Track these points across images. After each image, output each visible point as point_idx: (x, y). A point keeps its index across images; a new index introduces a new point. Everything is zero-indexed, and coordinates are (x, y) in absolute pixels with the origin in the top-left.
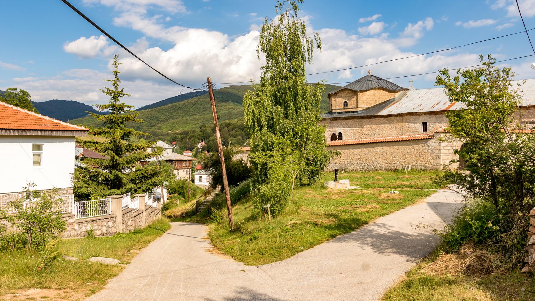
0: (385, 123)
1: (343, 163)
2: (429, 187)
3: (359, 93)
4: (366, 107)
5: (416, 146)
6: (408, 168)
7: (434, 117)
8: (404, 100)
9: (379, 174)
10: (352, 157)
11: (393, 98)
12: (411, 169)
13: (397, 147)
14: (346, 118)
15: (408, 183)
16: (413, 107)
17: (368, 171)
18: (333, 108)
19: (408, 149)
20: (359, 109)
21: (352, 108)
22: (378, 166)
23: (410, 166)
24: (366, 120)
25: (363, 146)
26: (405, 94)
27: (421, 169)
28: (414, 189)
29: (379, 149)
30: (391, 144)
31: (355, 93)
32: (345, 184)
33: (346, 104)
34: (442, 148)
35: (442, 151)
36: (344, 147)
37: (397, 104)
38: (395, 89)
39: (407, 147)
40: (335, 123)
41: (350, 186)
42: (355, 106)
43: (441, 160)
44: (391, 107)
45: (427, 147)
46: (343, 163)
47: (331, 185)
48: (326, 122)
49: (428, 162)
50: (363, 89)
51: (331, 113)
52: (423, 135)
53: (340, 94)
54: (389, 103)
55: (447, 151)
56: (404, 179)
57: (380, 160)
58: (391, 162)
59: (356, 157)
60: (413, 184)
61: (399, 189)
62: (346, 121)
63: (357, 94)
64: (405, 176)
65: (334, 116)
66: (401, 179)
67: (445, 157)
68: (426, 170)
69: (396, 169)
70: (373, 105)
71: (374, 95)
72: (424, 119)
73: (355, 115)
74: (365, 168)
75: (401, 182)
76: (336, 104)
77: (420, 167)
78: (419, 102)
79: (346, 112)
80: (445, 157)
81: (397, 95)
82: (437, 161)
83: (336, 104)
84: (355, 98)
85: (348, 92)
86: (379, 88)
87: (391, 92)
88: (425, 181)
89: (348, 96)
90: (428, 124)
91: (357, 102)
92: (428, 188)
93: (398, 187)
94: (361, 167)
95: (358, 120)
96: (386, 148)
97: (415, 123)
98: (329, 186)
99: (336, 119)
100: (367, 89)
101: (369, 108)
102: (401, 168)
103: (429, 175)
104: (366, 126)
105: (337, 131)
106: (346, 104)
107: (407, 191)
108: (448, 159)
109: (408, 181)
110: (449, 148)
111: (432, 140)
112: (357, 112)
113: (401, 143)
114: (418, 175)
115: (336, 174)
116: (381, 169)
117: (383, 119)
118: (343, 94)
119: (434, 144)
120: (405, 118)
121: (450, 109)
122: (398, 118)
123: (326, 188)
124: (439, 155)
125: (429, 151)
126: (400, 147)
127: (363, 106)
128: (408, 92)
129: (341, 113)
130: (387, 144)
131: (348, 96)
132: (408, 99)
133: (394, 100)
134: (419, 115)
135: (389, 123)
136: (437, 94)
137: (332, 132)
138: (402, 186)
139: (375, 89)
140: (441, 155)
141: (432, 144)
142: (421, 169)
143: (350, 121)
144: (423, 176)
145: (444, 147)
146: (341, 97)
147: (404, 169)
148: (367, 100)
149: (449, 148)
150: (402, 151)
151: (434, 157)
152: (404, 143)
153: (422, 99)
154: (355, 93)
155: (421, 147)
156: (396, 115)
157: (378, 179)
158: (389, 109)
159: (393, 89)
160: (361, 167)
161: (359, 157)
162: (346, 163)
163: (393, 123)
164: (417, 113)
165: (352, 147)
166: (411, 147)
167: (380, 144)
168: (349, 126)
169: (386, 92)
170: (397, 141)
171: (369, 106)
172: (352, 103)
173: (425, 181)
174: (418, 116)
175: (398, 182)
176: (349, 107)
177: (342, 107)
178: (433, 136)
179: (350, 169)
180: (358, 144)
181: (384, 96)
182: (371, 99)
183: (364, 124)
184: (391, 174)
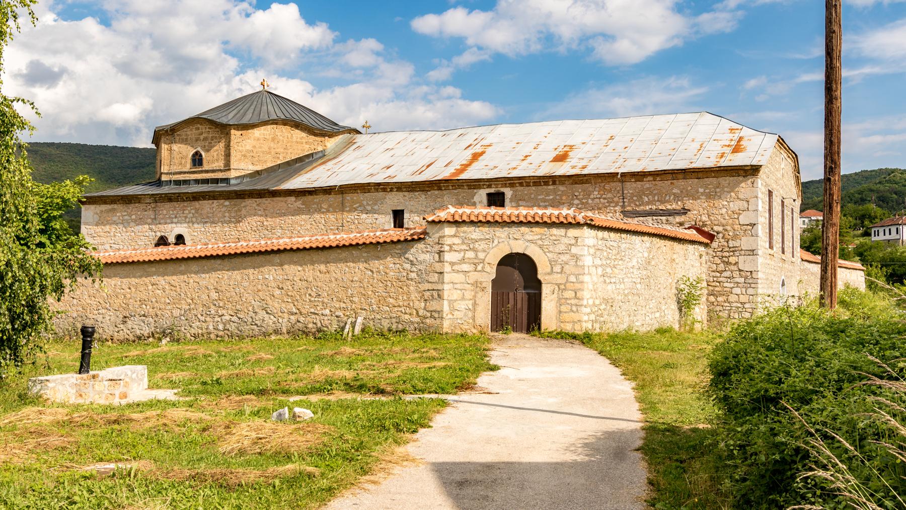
0: (298, 212)
1: (167, 314)
2: (420, 385)
3: (233, 132)
4: (252, 168)
5: (376, 264)
6: (353, 325)
7: (421, 197)
8: (349, 155)
9: (271, 344)
10: (195, 296)
11: (320, 149)
12: (363, 330)
13: (322, 267)
14: (196, 197)
15: (348, 374)
16: (370, 171)
17: (241, 338)
18: (164, 169)
19: (353, 271)
20: (233, 174)
21: (213, 171)
22: (270, 321)
23: (360, 320)
24: (250, 203)
25: (226, 262)
26: (351, 143)
27: (390, 330)
28: (368, 397)
29: (271, 274)
30: (307, 256)
31: (223, 129)
32: (125, 383)
33: (197, 160)
34: (447, 268)
35: (447, 277)
36: (171, 267)
37: (330, 164)
38: (327, 129)
39: (352, 264)
40: (166, 209)
41: (150, 388)
42: (220, 164)
43: (446, 303)
44: (314, 172)
45: (408, 266)
46: (167, 314)
47: (62, 388)
48: (142, 206)
49: (407, 307)
50: (245, 121)
51: (159, 183)
52: (396, 234)
53: (182, 133)
54: (311, 163)
55: (460, 277)
56: (339, 358)
57: (275, 305)
58: (306, 308)
59: (204, 297)
60: (367, 375)
61: (314, 398)
62: (196, 204)
63: (228, 134)
64: (343, 348)
65: (165, 190)
66: (332, 361)
67: (456, 295)
68: (403, 331)
69: (319, 330)
70: (270, 165)
71: (273, 139)
72: (395, 200)
73: (221, 187)
74: (232, 327)
75: (328, 371)
76: (171, 158)
77: (386, 324)
78: (385, 160)
79: (197, 181)
80: (456, 295)
81: (331, 144)
82: (433, 305)
83: (171, 158)
84: (222, 145)
85: (204, 128)
86: (285, 122)
87: (316, 135)
88: (404, 366)
89: (205, 139)
90: (406, 216)
91: (228, 155)
92: (416, 390)
93: (313, 390)
94: (221, 327)
95: (227, 203)
96: (293, 270)
97: (374, 212)
98: (48, 393)
99: (169, 198)
100: (255, 120)
101: (258, 173)
102: (335, 326)
103: (412, 345)
104: (249, 219)
105: (172, 231)
106: (197, 160)
107: (345, 407)
108: (463, 299)
109: (350, 365)
110: (465, 267)
111: (420, 246)
112: (226, 180)
113: (333, 254)
114: (382, 346)
115: (86, 346)
116: (276, 332)
117: (293, 199)
118: (191, 132)
119: (427, 257)
120: (348, 197)
121: (463, 176)
122: (332, 198)
123: (37, 400)
124: (439, 287)
125: (413, 275)
126: (332, 267)
127: (242, 165)
128: (360, 139)
129: (186, 182)
130: (295, 257)
131: (205, 139)
132: (358, 153)
133: (323, 154)
134: (384, 190)
135: (308, 211)
136: (427, 144)
137: (159, 234)
138: (326, 386)
139: (275, 122)
140: (446, 287)
141: (422, 257)
142: (390, 330)
143: (206, 206)
144: (397, 348)
145: (452, 264)
146: (185, 141)
147: (343, 329)
148: (252, 152)
149: (465, 267)
150: (339, 276)
151: (427, 294)
152: (344, 254)
153: (392, 153)
154: (223, 129)
155: (389, 265)
156: (328, 191)
157: (259, 361)
158: (309, 175)
159: (322, 128)
160: (221, 327)
161: (214, 295)
162: (176, 313)
163: (319, 211)
164: (379, 184)
165: (194, 266)
166: (362, 266)
167: (277, 258)
168: (206, 220)
169: (304, 135)
170: (324, 248)
171: (259, 168)
172: (213, 159)
173: (404, 366)
174: (381, 194)
175: (319, 372)
176: (206, 167)
177: (188, 167)
178: (425, 233)
179: (187, 332)
180: (212, 257)
181: (298, 143)
182: (265, 148)
183: (244, 212)
184: (305, 345)
